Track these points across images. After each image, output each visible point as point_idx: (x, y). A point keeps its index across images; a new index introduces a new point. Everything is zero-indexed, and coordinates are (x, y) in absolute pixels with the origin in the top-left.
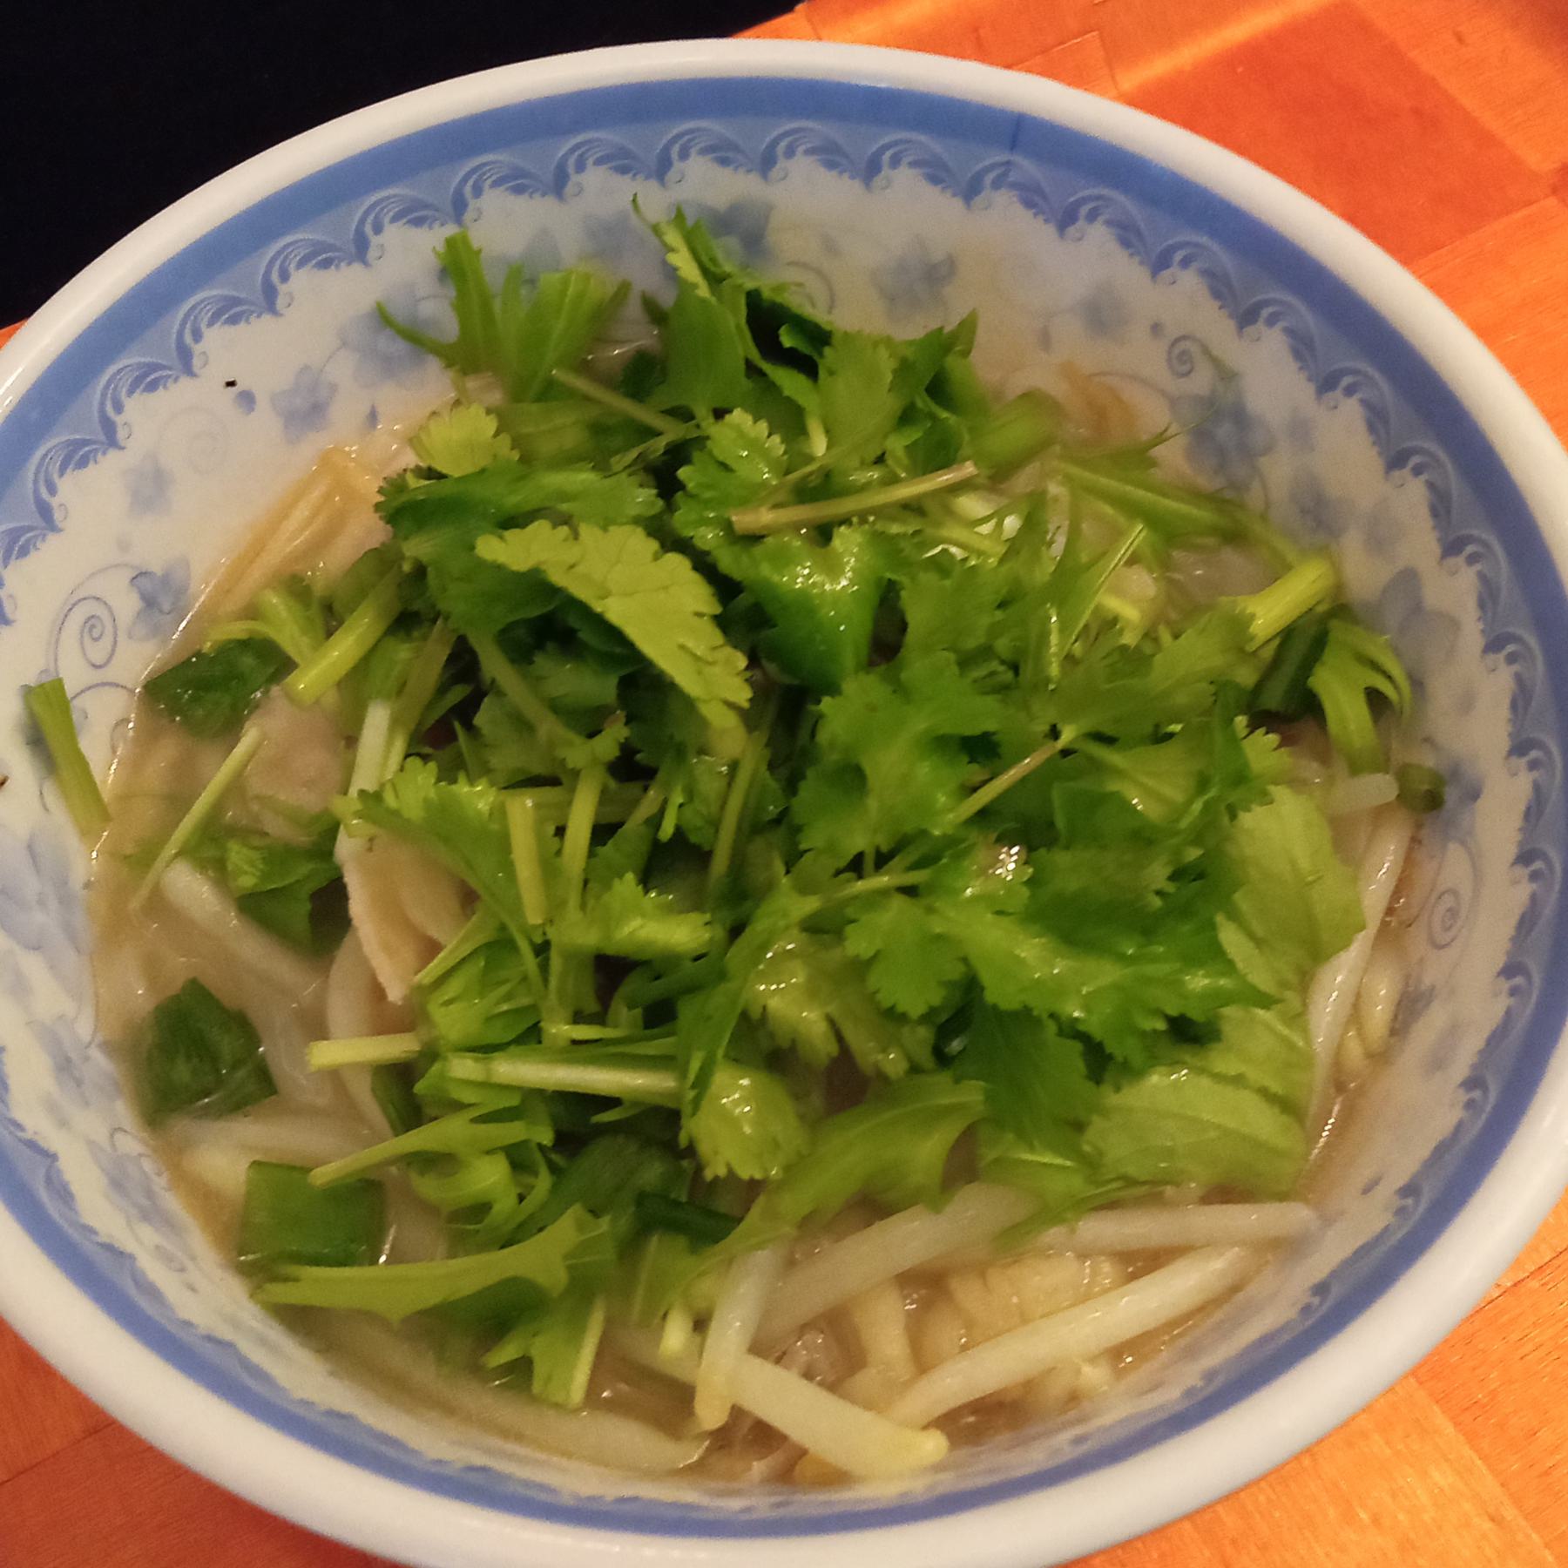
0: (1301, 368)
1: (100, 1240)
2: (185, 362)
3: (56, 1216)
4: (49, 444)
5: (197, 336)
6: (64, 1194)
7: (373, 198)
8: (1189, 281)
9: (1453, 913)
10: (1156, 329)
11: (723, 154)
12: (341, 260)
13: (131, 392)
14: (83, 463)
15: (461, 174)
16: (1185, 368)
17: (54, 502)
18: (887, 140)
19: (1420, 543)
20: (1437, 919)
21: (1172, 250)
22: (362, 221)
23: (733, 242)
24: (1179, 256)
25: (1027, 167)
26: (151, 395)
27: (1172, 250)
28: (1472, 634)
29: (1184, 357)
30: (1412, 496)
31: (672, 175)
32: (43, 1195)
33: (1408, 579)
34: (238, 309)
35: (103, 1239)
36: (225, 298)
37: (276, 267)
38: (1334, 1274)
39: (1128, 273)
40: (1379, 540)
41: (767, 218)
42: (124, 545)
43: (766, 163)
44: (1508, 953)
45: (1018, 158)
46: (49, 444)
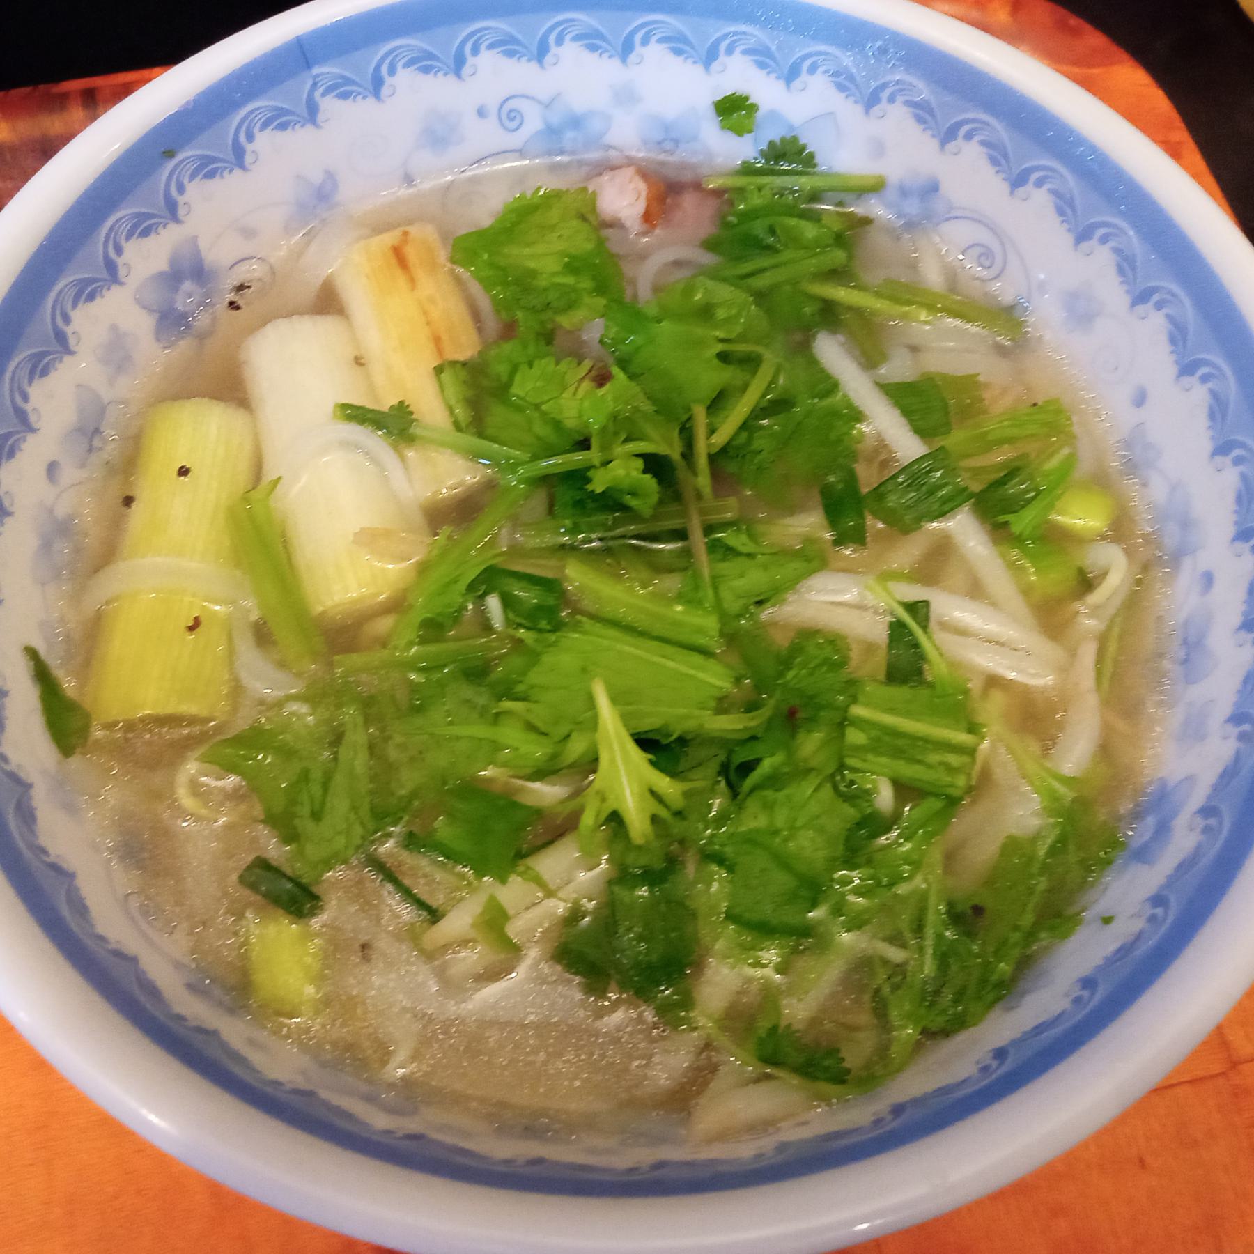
0: (1210, 427)
1: (110, 947)
2: (112, 273)
3: (75, 929)
4: (17, 360)
6: (81, 909)
7: (823, 48)
12: (102, 287)
13: (74, 306)
14: (91, 297)
15: (549, 24)
17: (69, 330)
18: (970, 115)
21: (1153, 290)
22: (464, 43)
23: (187, 286)
26: (145, 239)
27: (1153, 290)
32: (65, 912)
34: (284, 119)
35: (113, 946)
41: (197, 253)
43: (172, 211)
45: (316, 70)
46: (17, 360)
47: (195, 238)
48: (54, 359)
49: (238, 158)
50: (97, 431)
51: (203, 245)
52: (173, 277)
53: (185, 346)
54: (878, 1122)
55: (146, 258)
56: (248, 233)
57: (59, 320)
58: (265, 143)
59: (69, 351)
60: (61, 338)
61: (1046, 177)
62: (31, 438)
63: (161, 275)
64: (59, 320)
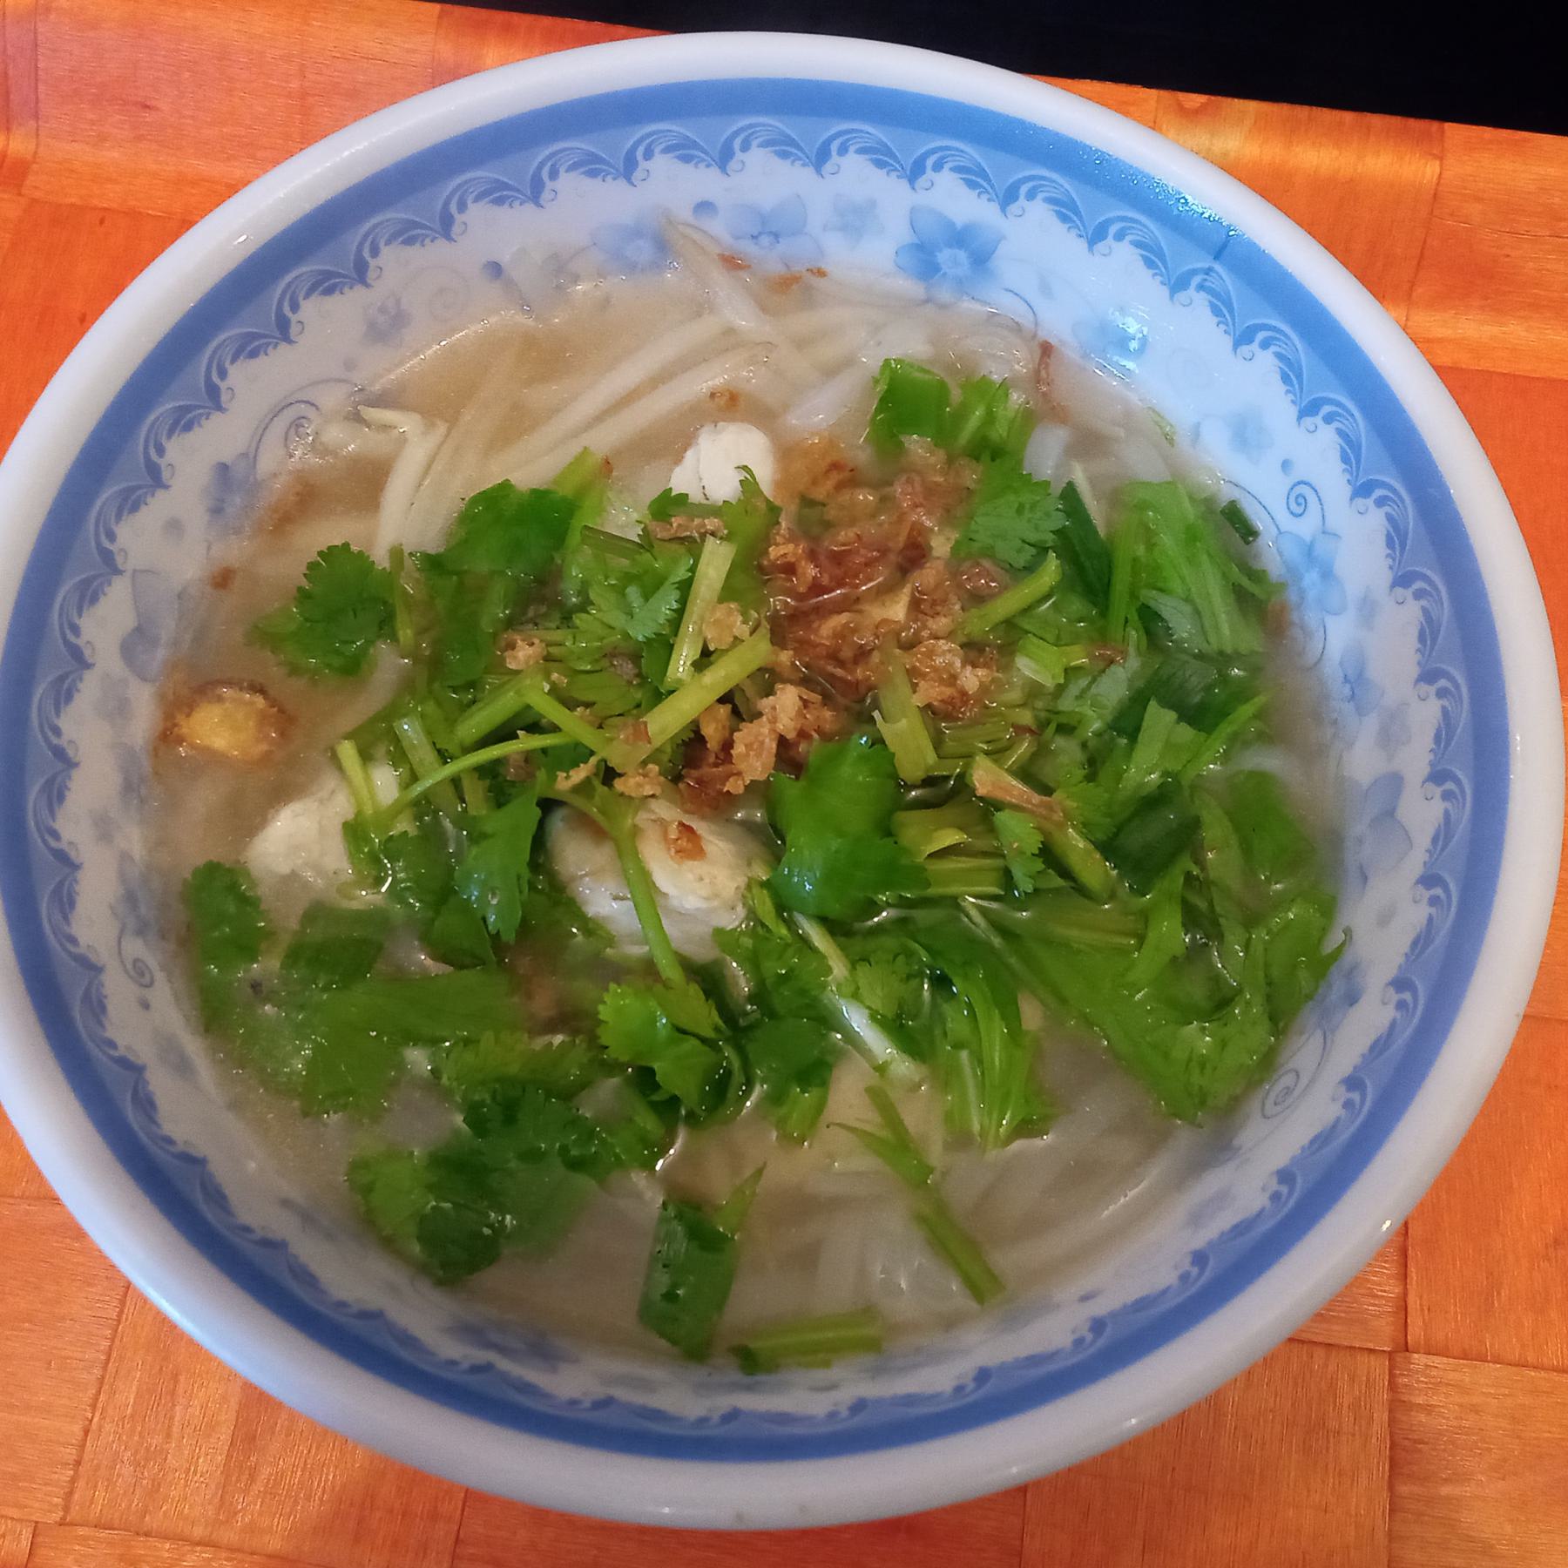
5: (554, 175)
8: (1327, 437)
9: (1288, 1091)
10: (1286, 465)
11: (974, 178)
16: (1299, 510)
19: (1416, 759)
20: (1272, 1096)
23: (962, 255)
24: (1326, 409)
25: (1225, 278)
28: (1415, 863)
29: (1302, 500)
30: (1425, 714)
31: (922, 182)
33: (1394, 783)
36: (408, 221)
37: (367, 244)
38: (1113, 1315)
39: (1278, 407)
40: (1389, 738)
42: (349, 365)
43: (1008, 198)
44: (1293, 1158)
45: (1217, 267)
47: (1004, 237)
48: (201, 415)
49: (1096, 237)
50: (776, 236)
51: (1003, 249)
52: (960, 237)
53: (908, 286)
54: (703, 1421)
55: (951, 198)
56: (1045, 289)
57: (152, 452)
58: (1124, 254)
59: (286, 337)
60: (213, 392)
61: (650, 145)
62: (216, 417)
63: (950, 225)
64: (152, 452)
